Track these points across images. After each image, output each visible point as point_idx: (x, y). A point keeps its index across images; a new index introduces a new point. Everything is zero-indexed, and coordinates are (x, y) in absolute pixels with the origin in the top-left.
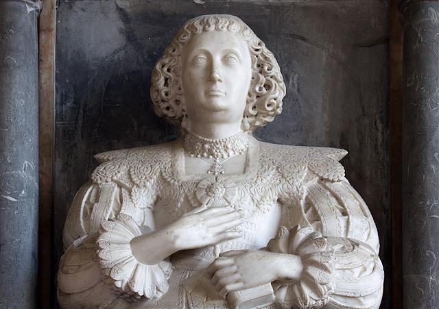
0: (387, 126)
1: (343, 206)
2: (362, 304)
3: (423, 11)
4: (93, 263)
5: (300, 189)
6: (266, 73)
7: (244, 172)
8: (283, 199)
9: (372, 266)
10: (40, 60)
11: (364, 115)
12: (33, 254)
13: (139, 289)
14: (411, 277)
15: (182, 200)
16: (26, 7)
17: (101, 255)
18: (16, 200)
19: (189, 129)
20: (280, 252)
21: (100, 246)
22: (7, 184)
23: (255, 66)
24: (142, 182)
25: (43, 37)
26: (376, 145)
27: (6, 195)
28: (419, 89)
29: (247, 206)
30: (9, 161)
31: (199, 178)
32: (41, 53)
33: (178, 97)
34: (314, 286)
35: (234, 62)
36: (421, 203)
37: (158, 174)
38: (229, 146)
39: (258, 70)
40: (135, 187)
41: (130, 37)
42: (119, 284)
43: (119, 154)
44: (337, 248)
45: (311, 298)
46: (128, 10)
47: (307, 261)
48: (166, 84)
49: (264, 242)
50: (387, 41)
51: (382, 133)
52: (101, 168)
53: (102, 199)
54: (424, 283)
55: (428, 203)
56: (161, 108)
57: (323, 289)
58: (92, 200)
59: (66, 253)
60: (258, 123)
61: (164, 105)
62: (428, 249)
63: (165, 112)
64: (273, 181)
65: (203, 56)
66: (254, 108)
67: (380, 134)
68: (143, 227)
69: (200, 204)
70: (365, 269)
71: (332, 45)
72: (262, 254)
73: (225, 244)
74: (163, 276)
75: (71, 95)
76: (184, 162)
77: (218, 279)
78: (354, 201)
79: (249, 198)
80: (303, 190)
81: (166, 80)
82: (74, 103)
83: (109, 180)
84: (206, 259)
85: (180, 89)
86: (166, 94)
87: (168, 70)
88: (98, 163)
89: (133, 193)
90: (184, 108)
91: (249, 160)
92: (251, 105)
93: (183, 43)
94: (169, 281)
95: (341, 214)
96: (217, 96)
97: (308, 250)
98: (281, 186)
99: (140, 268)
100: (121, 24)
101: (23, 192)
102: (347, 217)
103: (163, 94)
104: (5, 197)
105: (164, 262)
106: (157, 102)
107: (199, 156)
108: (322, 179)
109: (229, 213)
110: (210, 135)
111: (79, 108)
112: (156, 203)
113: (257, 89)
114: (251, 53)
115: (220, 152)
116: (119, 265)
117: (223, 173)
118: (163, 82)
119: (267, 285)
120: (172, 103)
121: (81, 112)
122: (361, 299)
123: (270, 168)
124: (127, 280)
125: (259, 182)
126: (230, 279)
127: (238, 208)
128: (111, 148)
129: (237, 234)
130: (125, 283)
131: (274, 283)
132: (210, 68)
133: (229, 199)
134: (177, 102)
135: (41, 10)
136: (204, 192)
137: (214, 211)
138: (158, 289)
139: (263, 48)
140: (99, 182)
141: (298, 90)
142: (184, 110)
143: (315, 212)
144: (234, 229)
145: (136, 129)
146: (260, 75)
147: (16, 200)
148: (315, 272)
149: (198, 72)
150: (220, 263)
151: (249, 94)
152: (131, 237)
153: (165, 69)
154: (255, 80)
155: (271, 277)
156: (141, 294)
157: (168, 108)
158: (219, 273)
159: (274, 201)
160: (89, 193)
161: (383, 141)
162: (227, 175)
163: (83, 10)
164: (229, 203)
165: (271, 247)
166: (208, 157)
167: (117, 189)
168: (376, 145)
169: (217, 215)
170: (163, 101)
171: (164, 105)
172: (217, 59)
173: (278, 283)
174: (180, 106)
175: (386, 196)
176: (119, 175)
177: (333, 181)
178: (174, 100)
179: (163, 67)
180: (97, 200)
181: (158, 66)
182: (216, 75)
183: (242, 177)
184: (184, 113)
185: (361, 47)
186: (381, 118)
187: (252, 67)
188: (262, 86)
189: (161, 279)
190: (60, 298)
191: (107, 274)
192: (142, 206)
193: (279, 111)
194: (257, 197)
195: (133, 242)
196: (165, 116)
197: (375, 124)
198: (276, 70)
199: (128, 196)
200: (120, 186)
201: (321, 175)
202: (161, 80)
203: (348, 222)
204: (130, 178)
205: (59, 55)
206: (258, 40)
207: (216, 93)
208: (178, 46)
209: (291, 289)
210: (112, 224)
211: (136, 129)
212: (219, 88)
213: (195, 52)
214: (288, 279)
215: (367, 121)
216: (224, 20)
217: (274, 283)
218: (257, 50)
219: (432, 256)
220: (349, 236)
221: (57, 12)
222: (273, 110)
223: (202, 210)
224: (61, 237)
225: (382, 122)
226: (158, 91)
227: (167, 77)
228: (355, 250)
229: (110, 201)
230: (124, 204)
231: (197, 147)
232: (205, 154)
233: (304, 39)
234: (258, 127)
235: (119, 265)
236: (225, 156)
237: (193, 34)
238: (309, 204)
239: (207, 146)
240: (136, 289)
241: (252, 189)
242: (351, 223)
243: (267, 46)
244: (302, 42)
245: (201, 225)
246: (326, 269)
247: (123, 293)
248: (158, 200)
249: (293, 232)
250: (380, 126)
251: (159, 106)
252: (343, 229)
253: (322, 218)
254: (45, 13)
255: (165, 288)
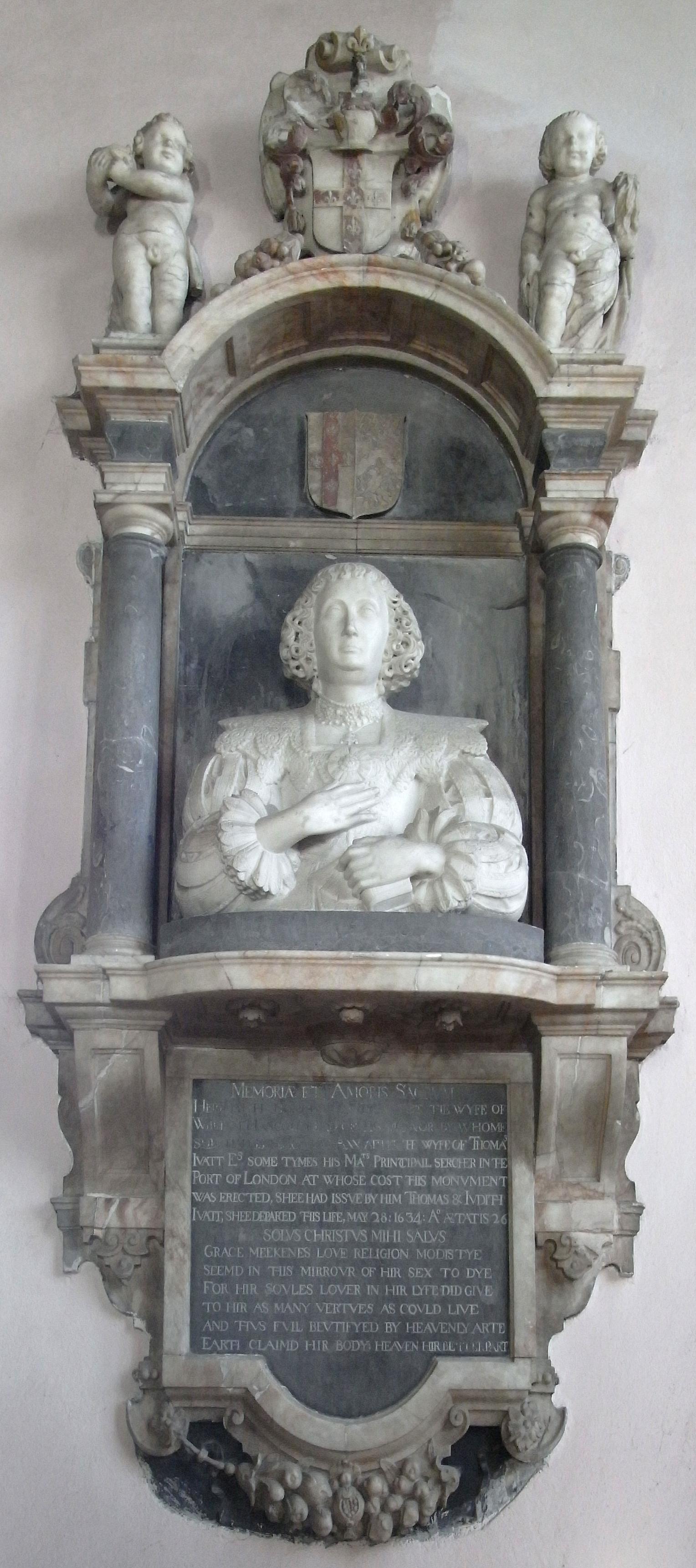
0: (525, 697)
1: (486, 785)
2: (506, 906)
3: (568, 566)
4: (214, 848)
5: (440, 764)
6: (403, 627)
7: (380, 742)
8: (421, 776)
9: (518, 859)
10: (163, 616)
11: (501, 684)
12: (150, 837)
13: (263, 882)
14: (558, 875)
15: (312, 774)
16: (150, 552)
17: (223, 840)
18: (131, 771)
19: (320, 692)
20: (419, 841)
21: (223, 828)
22: (124, 752)
23: (393, 621)
24: (269, 753)
25: (168, 589)
26: (513, 720)
27: (122, 764)
28: (565, 651)
29: (384, 783)
30: (126, 725)
31: (331, 748)
32: (166, 603)
33: (309, 655)
34: (457, 883)
35: (369, 613)
36: (568, 784)
37: (286, 744)
38: (363, 712)
39: (395, 625)
40: (261, 758)
41: (259, 593)
42: (242, 876)
43: (245, 720)
44: (481, 836)
45: (454, 898)
46: (257, 565)
47: (449, 850)
48: (296, 639)
49: (399, 827)
50: (525, 602)
51: (520, 705)
52: (225, 735)
53: (227, 771)
54: (572, 883)
55: (576, 784)
56: (291, 667)
57: (467, 887)
58: (215, 771)
59: (184, 837)
60: (393, 688)
61: (293, 664)
62: (575, 839)
63: (295, 672)
64: (411, 754)
65: (338, 607)
66: (390, 668)
67: (517, 706)
68: (270, 808)
69: (333, 780)
70: (511, 864)
71: (468, 606)
72: (400, 842)
73: (358, 829)
74: (290, 868)
75: (196, 656)
76: (314, 730)
77: (352, 872)
78: (498, 780)
79: (385, 774)
80: (442, 766)
81: (297, 634)
82: (199, 664)
83: (233, 749)
84: (336, 848)
85: (311, 645)
86: (297, 651)
87: (300, 623)
88: (221, 730)
89: (259, 766)
90: (316, 667)
91: (384, 731)
92: (387, 664)
93: (316, 593)
94: (296, 875)
95: (484, 795)
96: (352, 652)
97: (453, 836)
98: (419, 760)
99: (265, 858)
100: (249, 579)
101: (140, 762)
102: (491, 799)
103: (293, 651)
104: (121, 767)
105: (292, 850)
106: (287, 660)
107: (330, 723)
108: (463, 752)
109: (364, 791)
110: (342, 699)
111: (204, 669)
112: (283, 777)
113: (394, 647)
114: (389, 606)
115: (353, 718)
116: (242, 851)
117: (357, 743)
118: (294, 637)
119: (405, 880)
120: (302, 661)
121: (206, 674)
122: (507, 900)
123: (408, 739)
124: (251, 871)
125: (396, 755)
126: (363, 874)
127: (372, 785)
128: (235, 714)
129: (372, 817)
130: (249, 875)
131: (413, 878)
132: (345, 621)
133: (363, 774)
134: (308, 660)
135: (166, 558)
136: (336, 766)
137: (348, 788)
138: (285, 884)
139: (401, 600)
140: (223, 751)
141: (433, 655)
142: (315, 670)
143: (457, 792)
144: (368, 810)
145: (263, 695)
146: (398, 630)
147: (131, 771)
148: (460, 867)
149: (332, 625)
150: (354, 852)
151: (386, 652)
152: (255, 818)
153: (297, 622)
154: (392, 637)
155: (410, 871)
156: (266, 889)
157: (298, 668)
158: (352, 865)
159: (411, 777)
160: (212, 763)
161: (520, 714)
162: (359, 746)
163: (211, 563)
164: (364, 779)
165: (409, 834)
166: (341, 725)
167: (242, 761)
168: (513, 720)
169: (349, 793)
170: (293, 658)
171: (293, 664)
172: (353, 610)
173: (417, 877)
174: (311, 665)
175: (524, 777)
176: (244, 744)
177: (475, 755)
178: (305, 657)
179: (293, 620)
180: (220, 772)
181: (289, 618)
182: (352, 628)
183: (377, 749)
184: (316, 674)
185: (498, 609)
186: (519, 688)
187: (390, 622)
188: (400, 643)
189: (287, 870)
190: (177, 892)
191: (230, 863)
192: (268, 782)
193: (416, 674)
194: (394, 772)
195: (260, 823)
196: (295, 677)
197: (513, 696)
198: (415, 628)
199: (253, 769)
200: (245, 756)
201: (462, 748)
202: (291, 635)
203: (492, 805)
204: (256, 747)
205: (185, 613)
206: (397, 592)
207: (352, 649)
208: (311, 596)
209: (432, 885)
210: (236, 801)
211: (263, 695)
212: (355, 643)
213: (329, 602)
214: (428, 874)
215: (504, 691)
216: (360, 569)
217: (413, 878)
218: (395, 602)
219: (579, 847)
220: (494, 822)
221: (184, 565)
222: (411, 672)
223: (335, 785)
224: (181, 819)
225: (520, 693)
226: (288, 647)
227: (298, 631)
228: (501, 839)
229: (234, 774)
230: (249, 778)
231: (328, 713)
232: (337, 722)
233: (438, 599)
234: (393, 693)
235: (242, 851)
236: (359, 724)
237: (328, 582)
238: (450, 784)
239: (339, 712)
240: (261, 883)
241: (388, 763)
242: (495, 806)
243: (406, 600)
244: (436, 602)
245: (333, 805)
246: (471, 862)
247: (247, 888)
248: (286, 773)
249: (434, 815)
250: (517, 696)
251: (288, 666)
252: (487, 814)
253: (464, 799)
254: (170, 564)
255: (293, 883)
